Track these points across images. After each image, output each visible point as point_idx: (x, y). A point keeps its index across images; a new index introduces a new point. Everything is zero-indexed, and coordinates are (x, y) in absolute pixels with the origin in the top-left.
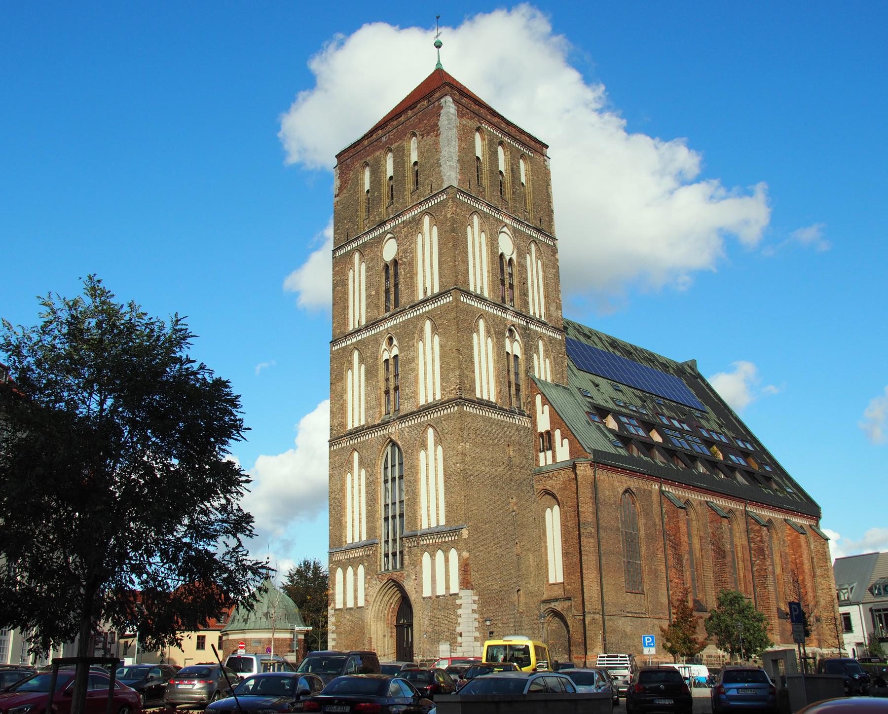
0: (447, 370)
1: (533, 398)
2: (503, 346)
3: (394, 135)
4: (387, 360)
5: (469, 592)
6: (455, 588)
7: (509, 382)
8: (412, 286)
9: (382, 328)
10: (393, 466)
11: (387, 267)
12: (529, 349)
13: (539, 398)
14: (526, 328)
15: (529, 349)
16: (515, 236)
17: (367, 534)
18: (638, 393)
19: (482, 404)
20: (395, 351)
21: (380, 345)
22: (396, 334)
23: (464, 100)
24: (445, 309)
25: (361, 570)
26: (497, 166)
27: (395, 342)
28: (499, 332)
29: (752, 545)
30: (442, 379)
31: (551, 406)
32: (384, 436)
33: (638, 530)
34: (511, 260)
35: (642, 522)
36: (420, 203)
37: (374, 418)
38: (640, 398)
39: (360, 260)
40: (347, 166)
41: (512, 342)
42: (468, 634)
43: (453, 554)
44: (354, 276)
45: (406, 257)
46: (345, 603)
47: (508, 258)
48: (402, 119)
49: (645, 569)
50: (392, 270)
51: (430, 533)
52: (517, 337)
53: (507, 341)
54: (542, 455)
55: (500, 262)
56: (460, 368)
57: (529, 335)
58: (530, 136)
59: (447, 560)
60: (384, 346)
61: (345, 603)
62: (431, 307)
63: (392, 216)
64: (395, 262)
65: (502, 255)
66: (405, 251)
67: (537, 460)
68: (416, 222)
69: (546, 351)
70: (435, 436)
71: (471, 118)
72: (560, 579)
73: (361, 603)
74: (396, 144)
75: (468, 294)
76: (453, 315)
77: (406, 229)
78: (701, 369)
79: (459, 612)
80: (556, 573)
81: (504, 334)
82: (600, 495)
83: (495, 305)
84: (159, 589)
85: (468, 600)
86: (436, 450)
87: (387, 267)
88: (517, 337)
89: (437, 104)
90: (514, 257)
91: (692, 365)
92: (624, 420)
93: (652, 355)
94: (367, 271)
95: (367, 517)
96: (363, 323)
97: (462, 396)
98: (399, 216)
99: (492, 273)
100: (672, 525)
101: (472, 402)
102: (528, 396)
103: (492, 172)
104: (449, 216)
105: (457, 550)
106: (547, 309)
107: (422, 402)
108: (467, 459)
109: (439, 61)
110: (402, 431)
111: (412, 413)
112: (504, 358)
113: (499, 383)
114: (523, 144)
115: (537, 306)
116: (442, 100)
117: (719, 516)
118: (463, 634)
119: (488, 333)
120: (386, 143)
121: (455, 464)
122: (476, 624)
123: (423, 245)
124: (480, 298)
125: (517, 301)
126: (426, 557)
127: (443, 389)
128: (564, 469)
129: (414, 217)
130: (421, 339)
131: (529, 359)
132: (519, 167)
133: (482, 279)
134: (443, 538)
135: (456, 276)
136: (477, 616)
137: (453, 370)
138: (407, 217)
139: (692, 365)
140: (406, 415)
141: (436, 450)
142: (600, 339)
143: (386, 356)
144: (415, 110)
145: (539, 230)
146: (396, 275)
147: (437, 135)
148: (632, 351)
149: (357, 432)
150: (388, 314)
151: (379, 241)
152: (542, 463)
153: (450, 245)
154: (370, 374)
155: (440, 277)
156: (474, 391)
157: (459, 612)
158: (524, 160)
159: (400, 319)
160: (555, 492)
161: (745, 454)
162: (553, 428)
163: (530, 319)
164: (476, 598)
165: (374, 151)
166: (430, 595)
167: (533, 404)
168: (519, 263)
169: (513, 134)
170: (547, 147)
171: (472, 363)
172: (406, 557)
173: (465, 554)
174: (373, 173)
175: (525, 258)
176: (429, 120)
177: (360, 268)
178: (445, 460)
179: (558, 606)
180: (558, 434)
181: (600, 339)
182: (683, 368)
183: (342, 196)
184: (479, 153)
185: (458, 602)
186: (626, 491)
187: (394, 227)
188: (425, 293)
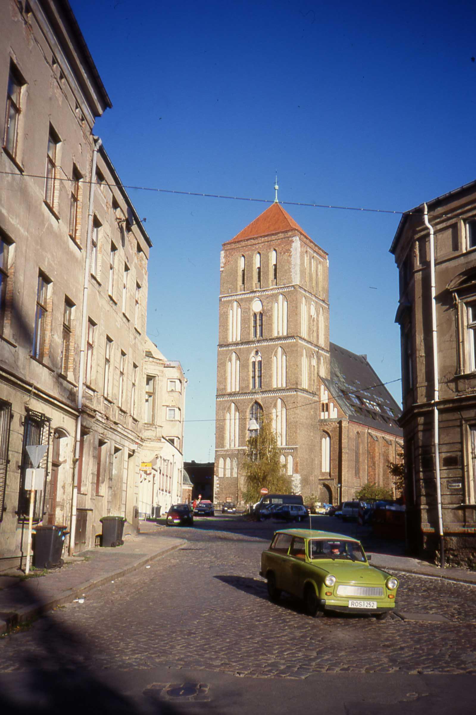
3: (263, 246)
4: (254, 363)
14: (318, 352)
19: (304, 390)
20: (259, 359)
21: (250, 353)
27: (259, 354)
46: (224, 475)
61: (224, 475)
64: (261, 314)
67: (320, 416)
75: (54, 181)
80: (326, 467)
88: (315, 357)
97: (293, 386)
100: (372, 448)
110: (263, 399)
117: (388, 443)
124: (304, 339)
128: (334, 422)
130: (276, 355)
151: (251, 300)
154: (243, 366)
160: (328, 431)
166: (276, 387)
177: (237, 311)
179: (327, 482)
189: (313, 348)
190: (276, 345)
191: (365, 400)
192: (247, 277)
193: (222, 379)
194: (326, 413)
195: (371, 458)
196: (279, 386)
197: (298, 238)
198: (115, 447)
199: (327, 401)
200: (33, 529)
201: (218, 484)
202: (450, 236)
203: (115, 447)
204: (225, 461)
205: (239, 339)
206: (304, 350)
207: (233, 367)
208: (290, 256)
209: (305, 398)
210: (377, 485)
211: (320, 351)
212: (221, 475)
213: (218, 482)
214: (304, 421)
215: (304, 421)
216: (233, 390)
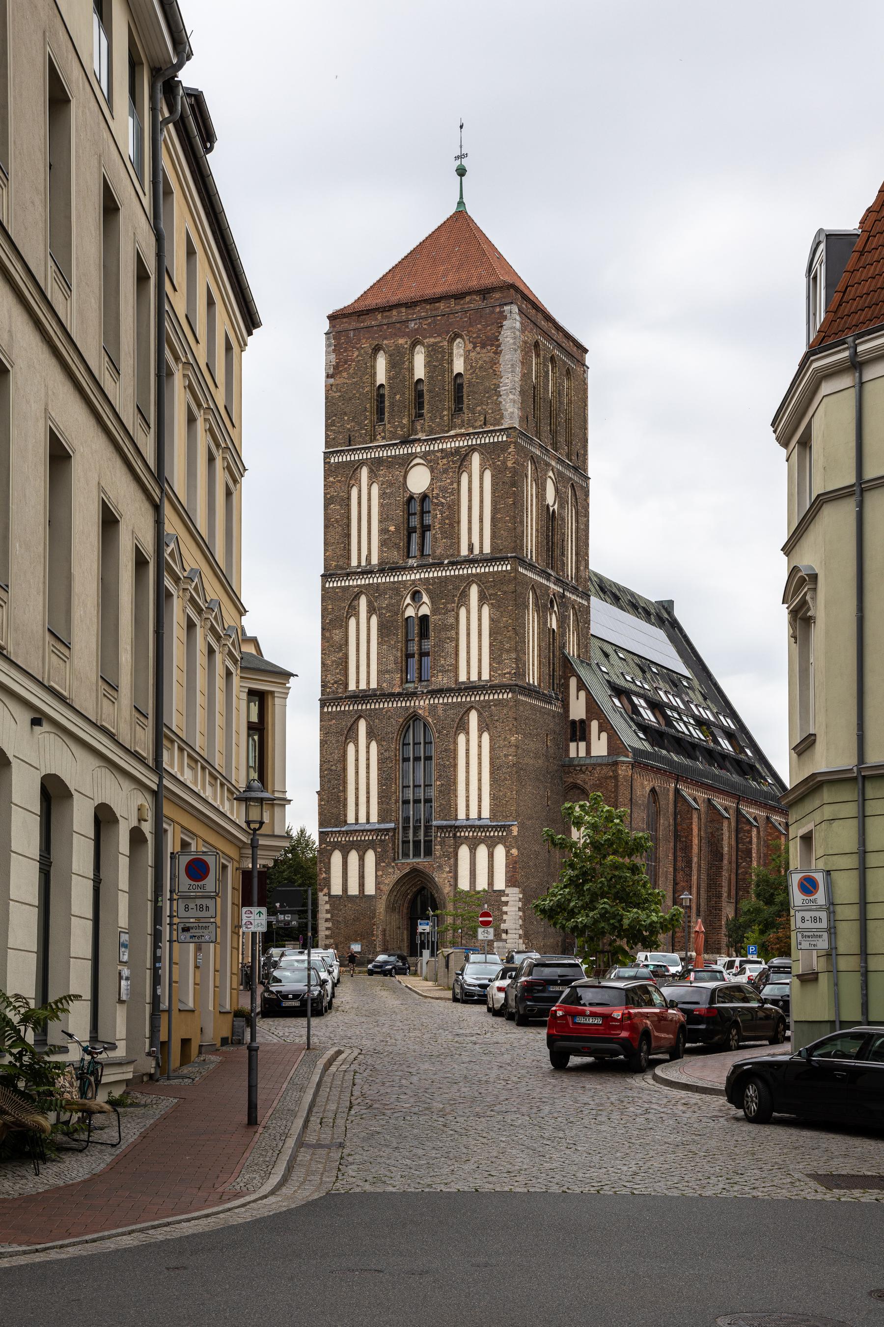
0: (499, 649)
1: (567, 680)
3: (429, 324)
5: (516, 890)
6: (500, 883)
13: (573, 682)
14: (563, 596)
17: (491, 810)
20: (425, 610)
24: (500, 579)
25: (370, 857)
27: (425, 599)
29: (740, 846)
31: (589, 695)
34: (554, 510)
36: (468, 434)
37: (390, 683)
39: (370, 478)
40: (349, 340)
42: (514, 931)
43: (500, 852)
44: (359, 498)
45: (444, 497)
52: (556, 608)
54: (573, 746)
56: (516, 650)
60: (408, 600)
64: (424, 497)
65: (548, 506)
68: (461, 459)
70: (479, 720)
73: (370, 889)
74: (432, 340)
76: (512, 587)
77: (445, 461)
84: (268, 881)
85: (514, 896)
86: (480, 737)
87: (411, 498)
88: (556, 608)
92: (123, 393)
95: (380, 797)
102: (560, 678)
104: (509, 464)
105: (505, 847)
108: (520, 751)
109: (461, 203)
110: (433, 708)
112: (544, 631)
116: (506, 308)
118: (509, 931)
121: (506, 756)
122: (520, 922)
126: (464, 852)
129: (458, 450)
135: (516, 541)
137: (508, 651)
141: (480, 737)
143: (410, 612)
151: (405, 463)
152: (572, 754)
153: (510, 501)
164: (521, 896)
167: (567, 687)
170: (586, 351)
173: (514, 851)
176: (485, 327)
180: (594, 725)
185: (504, 899)
190: (469, 580)
191: (669, 713)
192: (392, 404)
194: (582, 745)
195: (681, 849)
196: (474, 677)
197: (515, 309)
198: (182, 840)
200: (758, 896)
201: (327, 912)
202: (854, 395)
203: (182, 840)
204: (362, 859)
205: (374, 685)
207: (363, 630)
208: (498, 353)
209: (533, 707)
210: (77, 1020)
211: (567, 594)
212: (336, 889)
213: (328, 907)
214: (531, 762)
215: (531, 762)
216: (363, 686)
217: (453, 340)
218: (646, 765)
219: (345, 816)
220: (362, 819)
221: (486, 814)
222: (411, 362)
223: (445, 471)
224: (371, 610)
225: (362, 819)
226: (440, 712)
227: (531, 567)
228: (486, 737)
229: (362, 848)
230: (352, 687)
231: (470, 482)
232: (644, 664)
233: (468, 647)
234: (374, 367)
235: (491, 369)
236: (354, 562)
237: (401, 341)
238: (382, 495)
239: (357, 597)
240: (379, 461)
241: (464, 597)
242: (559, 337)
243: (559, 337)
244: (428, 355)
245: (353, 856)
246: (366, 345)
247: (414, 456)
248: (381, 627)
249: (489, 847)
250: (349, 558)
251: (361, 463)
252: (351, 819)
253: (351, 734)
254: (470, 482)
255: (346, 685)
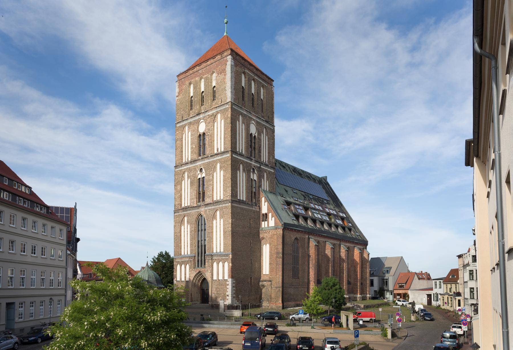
2: (250, 176)
4: (200, 178)
6: (226, 277)
7: (252, 192)
8: (212, 147)
9: (199, 163)
10: (202, 225)
11: (200, 135)
12: (260, 177)
15: (260, 177)
16: (257, 125)
17: (190, 252)
18: (303, 193)
20: (204, 175)
22: (204, 167)
23: (238, 57)
25: (188, 266)
26: (251, 91)
27: (204, 171)
28: (248, 170)
30: (224, 191)
32: (198, 212)
33: (298, 254)
34: (255, 136)
35: (300, 251)
38: (304, 196)
39: (188, 130)
41: (253, 174)
46: (181, 279)
47: (253, 135)
48: (209, 63)
49: (300, 269)
50: (202, 137)
51: (218, 255)
52: (256, 172)
53: (252, 174)
55: (250, 138)
57: (261, 171)
58: (266, 76)
59: (223, 266)
60: (199, 172)
61: (181, 279)
62: (220, 158)
63: (203, 111)
64: (204, 134)
65: (251, 134)
66: (209, 130)
68: (215, 116)
69: (267, 177)
71: (241, 67)
72: (268, 273)
74: (206, 76)
78: (329, 181)
79: (228, 287)
81: (250, 171)
82: (285, 241)
83: (247, 157)
86: (220, 221)
88: (256, 172)
89: (225, 58)
90: (256, 135)
91: (325, 178)
93: (310, 174)
94: (191, 136)
95: (190, 245)
96: (189, 160)
98: (206, 112)
99: (247, 143)
101: (237, 201)
103: (249, 94)
106: (269, 158)
107: (215, 199)
110: (206, 211)
111: (211, 204)
112: (250, 181)
113: (247, 192)
114: (263, 80)
115: (265, 157)
119: (244, 170)
120: (201, 74)
123: (221, 139)
124: (241, 155)
125: (257, 155)
127: (224, 195)
129: (213, 114)
131: (260, 181)
132: (260, 91)
133: (242, 146)
134: (221, 257)
136: (234, 288)
138: (210, 113)
139: (325, 178)
140: (208, 204)
141: (220, 221)
142: (289, 168)
143: (199, 177)
144: (215, 59)
145: (267, 122)
146: (204, 139)
147: (225, 75)
148: (302, 173)
149: (186, 209)
150: (200, 158)
151: (198, 122)
155: (224, 144)
156: (237, 196)
157: (228, 287)
158: (263, 87)
159: (206, 161)
161: (343, 219)
162: (269, 212)
163: (261, 163)
165: (195, 77)
168: (258, 137)
169: (259, 75)
170: (273, 81)
171: (237, 184)
172: (206, 263)
174: (195, 88)
175: (261, 135)
178: (224, 225)
181: (289, 168)
182: (321, 180)
183: (180, 97)
184: (243, 85)
185: (227, 283)
186: (296, 239)
187: (204, 117)
188: (218, 150)
189: (191, 166)
190: (216, 162)
193: (179, 193)
194: (266, 222)
199: (266, 212)
206: (241, 166)
216: (186, 205)
217: (212, 74)
218: (293, 229)
219: (181, 252)
220: (186, 254)
221: (222, 251)
222: (200, 86)
223: (209, 123)
224: (188, 177)
225: (186, 254)
226: (208, 212)
227: (241, 155)
228: (222, 220)
229: (185, 263)
230: (183, 206)
231: (217, 125)
232: (306, 195)
233: (217, 187)
234: (189, 90)
235: (223, 82)
236: (184, 161)
237: (197, 79)
238: (192, 135)
239: (184, 173)
240: (190, 123)
241: (215, 167)
242: (259, 73)
243: (259, 73)
244: (205, 82)
245: (183, 266)
246: (187, 83)
247: (200, 119)
248: (191, 183)
249: (223, 263)
250: (182, 160)
251: (185, 125)
252: (183, 254)
253: (182, 222)
254: (217, 125)
255: (181, 205)
